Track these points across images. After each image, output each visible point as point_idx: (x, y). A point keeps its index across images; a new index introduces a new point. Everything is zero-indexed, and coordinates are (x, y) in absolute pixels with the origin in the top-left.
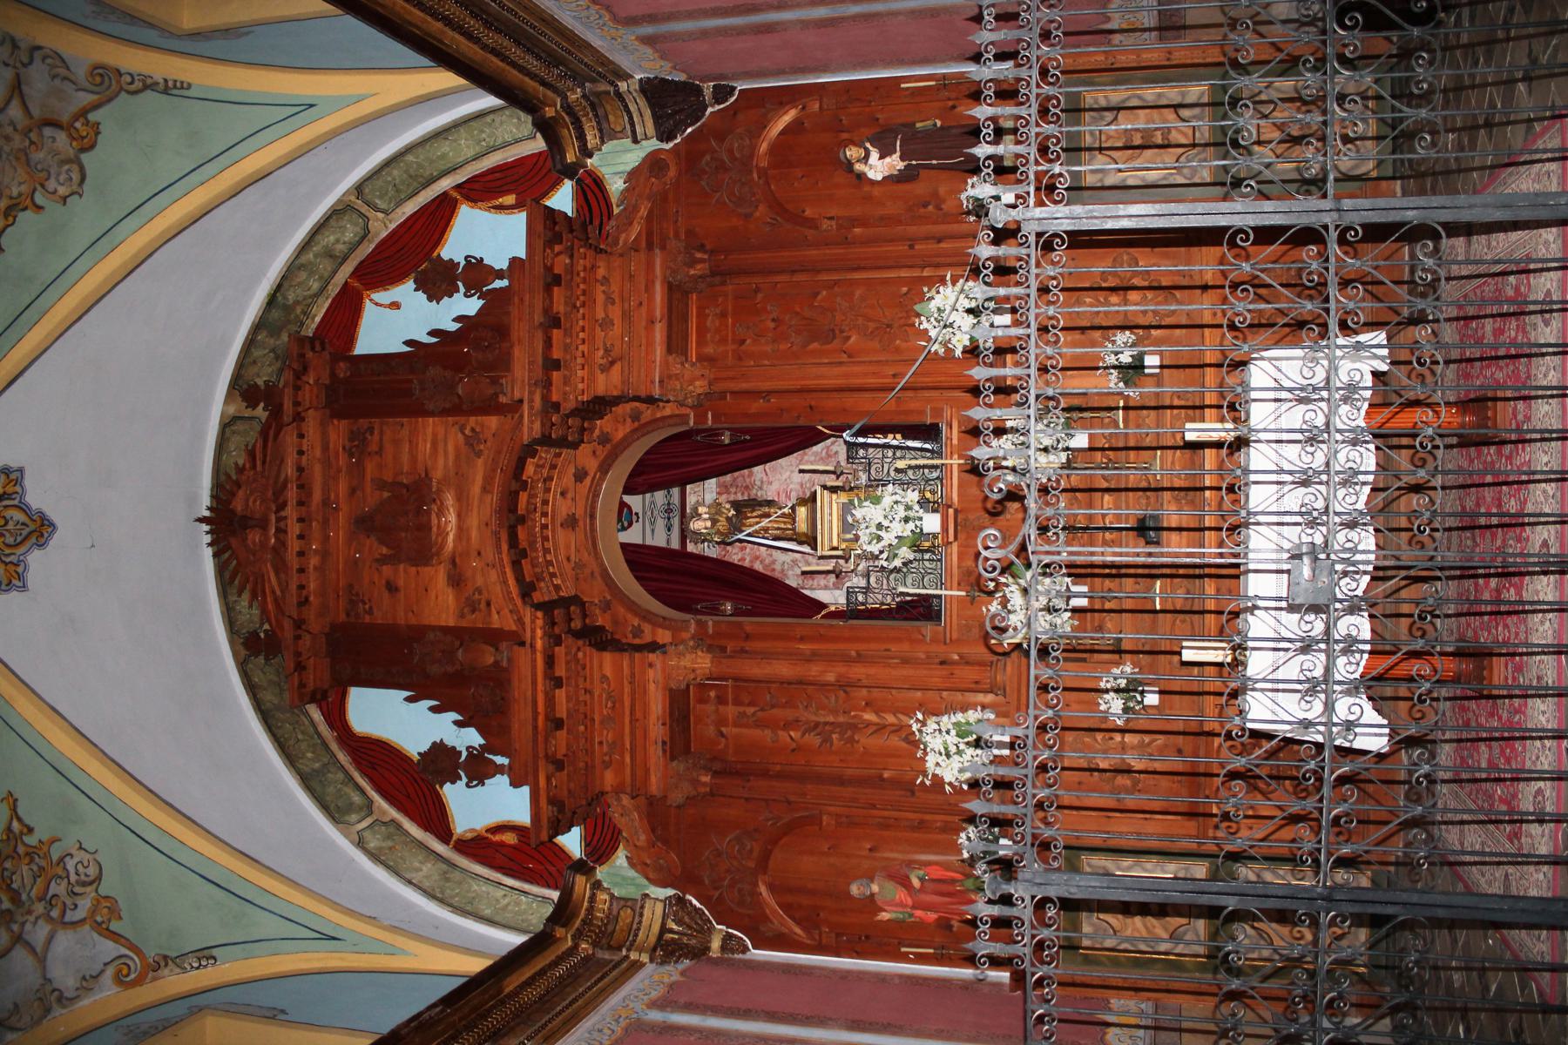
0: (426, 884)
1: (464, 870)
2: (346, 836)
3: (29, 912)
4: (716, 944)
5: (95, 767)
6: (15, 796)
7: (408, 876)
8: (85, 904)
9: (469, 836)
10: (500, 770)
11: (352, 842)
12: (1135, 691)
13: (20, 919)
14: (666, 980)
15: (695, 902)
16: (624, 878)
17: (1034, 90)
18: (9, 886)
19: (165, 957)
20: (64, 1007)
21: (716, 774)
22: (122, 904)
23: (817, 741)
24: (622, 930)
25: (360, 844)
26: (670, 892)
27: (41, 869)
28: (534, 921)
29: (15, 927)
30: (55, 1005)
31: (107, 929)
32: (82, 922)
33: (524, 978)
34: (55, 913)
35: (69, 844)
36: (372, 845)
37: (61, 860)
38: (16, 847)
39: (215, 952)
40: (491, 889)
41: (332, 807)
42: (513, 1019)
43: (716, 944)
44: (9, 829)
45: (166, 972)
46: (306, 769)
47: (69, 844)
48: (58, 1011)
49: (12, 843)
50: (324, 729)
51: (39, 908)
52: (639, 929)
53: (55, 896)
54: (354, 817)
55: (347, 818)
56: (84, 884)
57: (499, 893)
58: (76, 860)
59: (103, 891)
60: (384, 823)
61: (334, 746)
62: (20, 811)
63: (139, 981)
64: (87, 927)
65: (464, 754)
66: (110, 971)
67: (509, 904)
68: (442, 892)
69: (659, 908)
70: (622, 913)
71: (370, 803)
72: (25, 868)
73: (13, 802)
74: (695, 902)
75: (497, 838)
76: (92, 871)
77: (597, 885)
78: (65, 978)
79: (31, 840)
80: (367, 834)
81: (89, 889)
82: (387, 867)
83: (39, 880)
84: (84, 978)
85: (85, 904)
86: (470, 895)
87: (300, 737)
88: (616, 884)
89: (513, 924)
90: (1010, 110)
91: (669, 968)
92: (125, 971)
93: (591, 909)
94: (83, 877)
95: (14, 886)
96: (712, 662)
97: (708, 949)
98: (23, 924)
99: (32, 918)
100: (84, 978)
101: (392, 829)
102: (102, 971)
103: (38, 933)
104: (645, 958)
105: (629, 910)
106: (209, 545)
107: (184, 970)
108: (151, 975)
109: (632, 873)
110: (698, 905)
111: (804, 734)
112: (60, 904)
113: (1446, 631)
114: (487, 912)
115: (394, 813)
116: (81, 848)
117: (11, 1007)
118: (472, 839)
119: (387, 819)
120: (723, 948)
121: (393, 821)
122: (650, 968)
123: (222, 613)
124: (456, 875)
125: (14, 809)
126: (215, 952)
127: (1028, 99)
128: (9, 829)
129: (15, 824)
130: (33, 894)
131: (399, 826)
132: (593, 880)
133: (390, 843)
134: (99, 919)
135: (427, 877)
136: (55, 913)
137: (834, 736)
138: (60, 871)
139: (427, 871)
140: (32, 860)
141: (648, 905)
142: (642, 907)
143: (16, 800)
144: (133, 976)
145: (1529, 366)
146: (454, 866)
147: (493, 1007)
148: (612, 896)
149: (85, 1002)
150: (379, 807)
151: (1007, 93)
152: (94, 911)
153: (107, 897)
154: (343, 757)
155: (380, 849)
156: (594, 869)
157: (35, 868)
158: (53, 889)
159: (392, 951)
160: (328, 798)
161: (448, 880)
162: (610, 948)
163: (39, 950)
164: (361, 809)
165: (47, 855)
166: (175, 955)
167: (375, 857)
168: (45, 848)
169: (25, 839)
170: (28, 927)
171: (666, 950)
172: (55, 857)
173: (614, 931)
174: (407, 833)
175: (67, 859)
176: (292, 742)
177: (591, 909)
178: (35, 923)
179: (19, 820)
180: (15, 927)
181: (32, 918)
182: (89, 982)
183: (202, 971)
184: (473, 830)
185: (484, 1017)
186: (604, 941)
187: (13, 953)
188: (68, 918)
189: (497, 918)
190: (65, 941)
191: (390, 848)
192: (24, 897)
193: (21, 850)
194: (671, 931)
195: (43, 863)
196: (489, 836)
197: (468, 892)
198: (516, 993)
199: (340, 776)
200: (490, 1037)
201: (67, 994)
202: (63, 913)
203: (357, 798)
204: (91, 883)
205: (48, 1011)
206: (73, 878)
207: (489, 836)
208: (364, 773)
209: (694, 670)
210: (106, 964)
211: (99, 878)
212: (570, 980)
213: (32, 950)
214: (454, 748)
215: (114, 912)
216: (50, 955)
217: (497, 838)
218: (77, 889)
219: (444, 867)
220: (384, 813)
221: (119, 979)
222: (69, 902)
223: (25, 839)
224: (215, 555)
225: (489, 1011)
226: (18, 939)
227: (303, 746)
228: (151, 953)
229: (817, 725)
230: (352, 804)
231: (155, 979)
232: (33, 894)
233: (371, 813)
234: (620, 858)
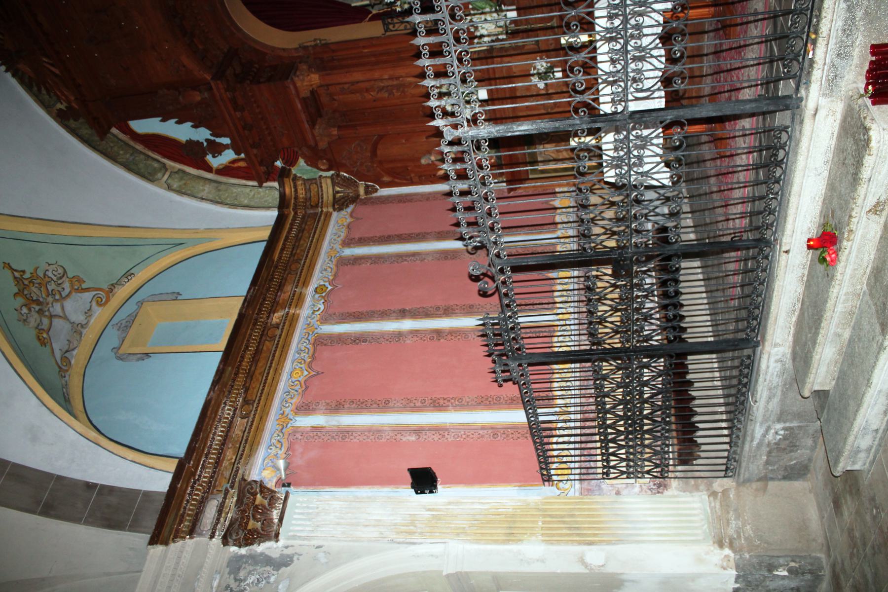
0: (211, 197)
1: (225, 183)
2: (161, 187)
3: (48, 304)
4: (362, 191)
5: (32, 228)
6: (7, 262)
7: (200, 196)
8: (67, 286)
9: (221, 167)
10: (226, 147)
11: (165, 189)
12: (550, 72)
13: (46, 309)
14: (345, 224)
15: (345, 174)
16: (307, 170)
17: (455, 69)
18: (32, 300)
19: (112, 285)
20: (86, 328)
21: (340, 128)
22: (82, 276)
23: (386, 95)
24: (314, 196)
25: (170, 188)
26: (332, 172)
27: (40, 284)
28: (270, 200)
29: (47, 313)
30: (82, 330)
31: (82, 289)
32: (70, 293)
33: (280, 247)
34: (57, 297)
35: (43, 267)
36: (175, 186)
37: (45, 275)
38: (23, 283)
39: (132, 271)
40: (243, 189)
41: (146, 175)
42: (284, 273)
43: (362, 191)
44: (15, 278)
45: (116, 290)
46: (124, 160)
47: (43, 267)
48: (84, 331)
49: (21, 282)
50: (121, 136)
51: (50, 299)
52: (322, 194)
53: (53, 290)
54: (159, 175)
55: (156, 177)
56: (61, 278)
57: (248, 190)
58: (51, 271)
59: (70, 275)
60: (176, 172)
61: (132, 143)
62: (14, 267)
63: (108, 300)
64: (74, 293)
65: (205, 144)
66: (94, 303)
67: (254, 195)
68: (220, 198)
69: (329, 181)
70: (311, 187)
71: (164, 165)
72: (33, 288)
73: (8, 266)
74: (345, 174)
75: (236, 165)
76: (61, 271)
77: (295, 178)
78: (80, 318)
79: (27, 275)
80: (169, 181)
81: (64, 279)
82: (188, 195)
83: (42, 289)
84: (86, 313)
85: (67, 286)
86: (235, 195)
87: (112, 145)
88: (303, 174)
89: (260, 205)
90: (444, 81)
91: (343, 213)
92: (100, 300)
93: (296, 198)
94: (58, 276)
95: (35, 298)
96: (320, 79)
97: (358, 196)
98: (49, 310)
99: (50, 305)
100: (86, 313)
101: (181, 174)
102: (91, 306)
103: (57, 309)
104: (331, 210)
105: (315, 185)
106: (7, 71)
107: (123, 285)
108: (111, 294)
109: (309, 168)
110: (347, 175)
111: (378, 93)
112: (57, 292)
113: (707, 65)
114: (246, 202)
115: (178, 166)
116: (49, 265)
117: (67, 342)
118: (223, 168)
119: (176, 170)
120: (366, 193)
121: (179, 170)
122: (335, 214)
123: (35, 101)
124: (222, 187)
125: (11, 268)
126: (132, 271)
127: (453, 74)
128: (15, 278)
129: (17, 274)
130: (44, 296)
131: (184, 172)
132: (292, 176)
133: (183, 182)
134: (76, 287)
135: (209, 193)
136: (57, 297)
137: (394, 91)
138: (47, 279)
139: (207, 190)
140: (33, 283)
141: (323, 181)
142: (321, 183)
143: (9, 264)
144: (104, 300)
145: (747, 27)
146: (220, 183)
147: (274, 272)
148: (304, 180)
149: (92, 321)
150: (171, 166)
151: (441, 73)
152: (72, 285)
153: (74, 277)
154: (139, 147)
155: (180, 186)
156: (290, 170)
157: (37, 285)
158: (50, 288)
159: (211, 240)
160: (142, 170)
161: (219, 190)
162: (312, 207)
163: (61, 314)
164: (161, 169)
165: (38, 277)
166: (115, 282)
167: (180, 192)
168: (35, 275)
169: (24, 277)
170: (51, 309)
171: (340, 204)
172: (41, 275)
173: (311, 197)
174: (190, 174)
175: (47, 273)
176: (109, 150)
177: (296, 198)
178: (53, 306)
179: (16, 271)
180: (47, 313)
181: (50, 305)
182: (88, 313)
183: (131, 281)
184: (222, 164)
185: (272, 280)
186: (308, 204)
187: (53, 323)
188: (64, 296)
189: (252, 204)
190: (69, 305)
191: (185, 184)
192: (41, 299)
193: (26, 282)
194: (338, 192)
195: (38, 281)
196: (232, 165)
197: (232, 193)
198: (280, 258)
199: (142, 157)
200: (278, 289)
201: (83, 323)
202: (61, 294)
203: (156, 165)
204: (63, 276)
205: (81, 334)
206: (55, 278)
207: (232, 165)
208: (153, 151)
209: (311, 85)
210: (91, 302)
211: (65, 272)
212: (300, 235)
213: (60, 317)
214: (198, 141)
215: (81, 281)
216: (67, 314)
217: (236, 165)
218: (59, 282)
219: (216, 185)
220: (173, 167)
221: (99, 304)
222: (60, 289)
223: (24, 277)
224: (14, 76)
225: (272, 275)
226: (51, 317)
227: (116, 149)
228: (105, 286)
229: (383, 87)
230: (155, 169)
231: (113, 296)
232: (44, 296)
233: (166, 170)
234: (301, 162)
